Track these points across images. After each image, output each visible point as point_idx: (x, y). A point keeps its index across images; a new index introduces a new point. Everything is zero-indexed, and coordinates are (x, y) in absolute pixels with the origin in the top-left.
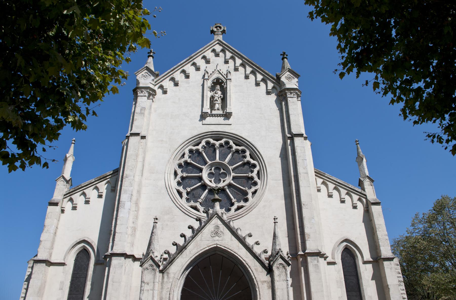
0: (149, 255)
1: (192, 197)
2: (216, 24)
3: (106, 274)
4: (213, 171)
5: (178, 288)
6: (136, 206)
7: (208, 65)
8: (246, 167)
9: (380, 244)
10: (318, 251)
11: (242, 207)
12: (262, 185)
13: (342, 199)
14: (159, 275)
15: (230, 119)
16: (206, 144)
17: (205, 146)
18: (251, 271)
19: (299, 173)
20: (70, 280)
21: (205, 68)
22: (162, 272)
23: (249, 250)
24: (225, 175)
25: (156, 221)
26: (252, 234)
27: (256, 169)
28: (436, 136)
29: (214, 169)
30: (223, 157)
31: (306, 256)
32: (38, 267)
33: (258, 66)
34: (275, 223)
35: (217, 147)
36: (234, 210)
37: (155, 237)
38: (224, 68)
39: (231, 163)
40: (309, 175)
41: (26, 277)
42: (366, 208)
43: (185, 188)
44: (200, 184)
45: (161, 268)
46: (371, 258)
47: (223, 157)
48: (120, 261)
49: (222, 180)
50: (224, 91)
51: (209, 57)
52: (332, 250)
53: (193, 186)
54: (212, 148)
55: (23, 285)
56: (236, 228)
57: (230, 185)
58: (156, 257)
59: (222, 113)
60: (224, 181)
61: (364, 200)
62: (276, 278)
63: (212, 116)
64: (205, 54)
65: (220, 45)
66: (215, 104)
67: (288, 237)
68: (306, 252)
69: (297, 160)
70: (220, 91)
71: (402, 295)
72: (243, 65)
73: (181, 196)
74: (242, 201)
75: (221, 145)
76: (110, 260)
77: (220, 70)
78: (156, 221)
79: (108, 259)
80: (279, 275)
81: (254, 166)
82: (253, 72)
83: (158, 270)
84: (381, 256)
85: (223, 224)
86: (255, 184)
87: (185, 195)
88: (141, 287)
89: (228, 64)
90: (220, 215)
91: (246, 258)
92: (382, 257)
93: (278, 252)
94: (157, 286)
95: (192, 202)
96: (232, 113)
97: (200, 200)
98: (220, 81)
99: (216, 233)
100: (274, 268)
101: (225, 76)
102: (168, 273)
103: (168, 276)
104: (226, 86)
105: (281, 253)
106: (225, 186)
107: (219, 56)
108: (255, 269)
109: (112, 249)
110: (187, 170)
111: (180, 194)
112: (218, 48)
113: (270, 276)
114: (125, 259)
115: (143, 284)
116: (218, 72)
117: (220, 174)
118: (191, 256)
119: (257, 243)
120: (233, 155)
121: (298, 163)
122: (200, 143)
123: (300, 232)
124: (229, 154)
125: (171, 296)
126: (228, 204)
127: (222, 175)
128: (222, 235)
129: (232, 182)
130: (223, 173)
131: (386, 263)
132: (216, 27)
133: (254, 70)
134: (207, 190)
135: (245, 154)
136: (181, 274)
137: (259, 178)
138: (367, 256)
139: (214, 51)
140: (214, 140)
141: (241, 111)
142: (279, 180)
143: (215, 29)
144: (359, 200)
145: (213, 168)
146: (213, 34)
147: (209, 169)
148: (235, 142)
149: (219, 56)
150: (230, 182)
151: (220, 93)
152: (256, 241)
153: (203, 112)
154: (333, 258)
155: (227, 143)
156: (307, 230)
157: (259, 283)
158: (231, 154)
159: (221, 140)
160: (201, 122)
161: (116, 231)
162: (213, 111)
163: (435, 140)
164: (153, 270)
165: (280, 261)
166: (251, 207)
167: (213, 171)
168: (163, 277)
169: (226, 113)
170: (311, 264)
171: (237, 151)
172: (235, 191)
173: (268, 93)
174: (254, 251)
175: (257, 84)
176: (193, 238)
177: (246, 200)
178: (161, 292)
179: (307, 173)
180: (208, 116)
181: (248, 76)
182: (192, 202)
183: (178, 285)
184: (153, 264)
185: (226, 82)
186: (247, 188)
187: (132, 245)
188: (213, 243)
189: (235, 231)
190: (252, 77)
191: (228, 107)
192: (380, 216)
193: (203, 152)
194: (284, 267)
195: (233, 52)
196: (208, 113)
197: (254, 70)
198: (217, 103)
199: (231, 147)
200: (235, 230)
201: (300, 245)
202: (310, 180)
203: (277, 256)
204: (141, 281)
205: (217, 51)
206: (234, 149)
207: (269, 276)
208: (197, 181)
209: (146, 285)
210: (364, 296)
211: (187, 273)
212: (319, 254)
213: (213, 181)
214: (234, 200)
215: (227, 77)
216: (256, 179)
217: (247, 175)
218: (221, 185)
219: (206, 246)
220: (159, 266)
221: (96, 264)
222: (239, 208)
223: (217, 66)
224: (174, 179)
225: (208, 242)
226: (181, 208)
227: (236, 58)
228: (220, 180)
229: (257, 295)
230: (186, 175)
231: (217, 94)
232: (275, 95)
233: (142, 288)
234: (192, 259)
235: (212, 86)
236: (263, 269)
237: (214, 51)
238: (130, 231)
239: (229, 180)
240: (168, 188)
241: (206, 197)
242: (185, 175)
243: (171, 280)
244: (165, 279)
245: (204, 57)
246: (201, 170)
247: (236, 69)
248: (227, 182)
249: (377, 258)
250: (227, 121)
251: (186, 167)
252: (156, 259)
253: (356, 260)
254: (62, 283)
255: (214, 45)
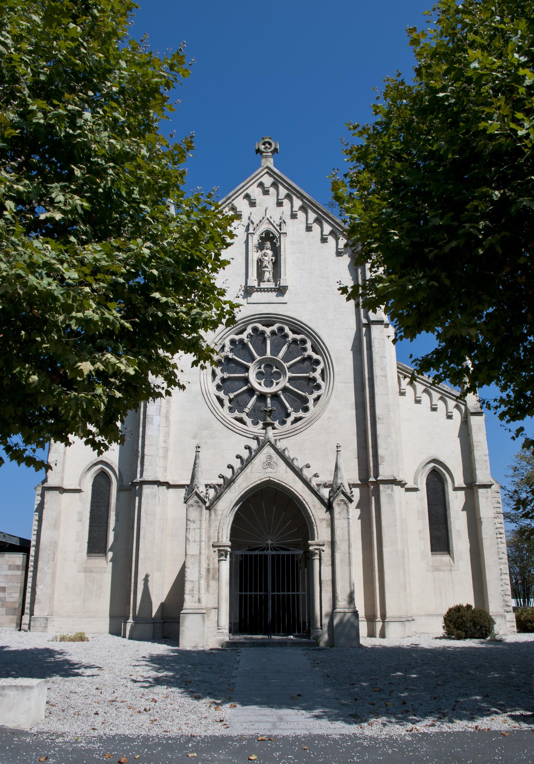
0: (193, 490)
1: (236, 405)
2: (263, 139)
3: (137, 504)
4: (262, 370)
5: (227, 526)
6: (166, 420)
7: (253, 209)
8: (307, 363)
9: (477, 466)
10: (393, 478)
11: (300, 418)
12: (327, 389)
13: (433, 406)
14: (205, 512)
15: (285, 295)
16: (252, 332)
17: (252, 334)
18: (308, 508)
19: (375, 375)
20: (89, 510)
21: (249, 215)
22: (208, 508)
23: (306, 483)
24: (278, 375)
25: (199, 450)
26: (311, 464)
27: (319, 366)
28: (486, 402)
29: (264, 367)
30: (276, 350)
31: (377, 483)
32: (49, 495)
33: (325, 211)
34: (337, 451)
35: (268, 335)
36: (290, 423)
37: (199, 469)
38: (275, 214)
39: (286, 358)
40: (389, 379)
41: (36, 507)
42: (464, 418)
43: (226, 393)
44: (245, 388)
45: (207, 505)
46: (465, 483)
47: (276, 350)
48: (153, 490)
49: (275, 381)
50: (276, 251)
51: (254, 196)
52: (415, 473)
53: (237, 390)
54: (260, 337)
55: (33, 516)
56: (292, 458)
57: (285, 390)
58: (202, 492)
59: (274, 286)
60: (277, 384)
61: (463, 407)
62: (336, 516)
63: (261, 291)
64: (248, 191)
65: (270, 175)
66: (264, 272)
67: (358, 458)
68: (379, 478)
69: (374, 358)
70: (271, 250)
71: (498, 530)
72: (303, 208)
73: (222, 405)
74: (301, 411)
75: (273, 333)
76: (141, 489)
77: (271, 217)
78: (199, 450)
79: (137, 487)
80: (340, 513)
81: (317, 362)
82: (318, 221)
83: (204, 507)
84: (476, 482)
85: (277, 453)
86: (318, 387)
87: (227, 404)
88: (187, 525)
89: (282, 206)
90: (273, 442)
91: (303, 493)
92: (477, 484)
93: (340, 487)
94: (204, 524)
95: (236, 412)
96: (287, 286)
97: (247, 410)
98: (271, 235)
99: (269, 464)
100: (335, 505)
101: (278, 228)
102: (215, 510)
103: (215, 513)
104: (279, 243)
105: (342, 488)
106: (278, 391)
107: (269, 194)
108: (313, 506)
109: (141, 475)
110: (228, 369)
111: (221, 401)
112: (267, 181)
113: (330, 514)
114: (158, 487)
115: (189, 522)
116: (267, 221)
117: (272, 374)
118: (241, 490)
119: (316, 476)
120: (289, 347)
121: (374, 362)
122: (245, 330)
123: (373, 453)
124: (284, 345)
125: (220, 535)
126: (283, 414)
127: (274, 375)
128: (275, 466)
129: (288, 385)
130: (275, 372)
131: (481, 491)
132: (264, 144)
133: (320, 217)
134: (255, 397)
135: (306, 345)
136: (230, 511)
137: (323, 380)
138: (460, 481)
139: (261, 185)
140: (263, 325)
141: (300, 282)
142: (350, 383)
143: (262, 147)
144: (457, 407)
145: (263, 366)
146: (259, 154)
147: (257, 367)
148: (292, 328)
149: (269, 194)
150: (285, 386)
151: (270, 253)
152: (315, 473)
153: (248, 285)
154: (415, 483)
155: (281, 329)
156: (380, 452)
157: (317, 521)
158: (286, 346)
159: (273, 325)
160: (246, 299)
161: (145, 453)
162: (262, 283)
163: (485, 405)
164: (199, 506)
165: (342, 497)
166: (312, 419)
167: (262, 370)
168: (210, 515)
169: (280, 287)
170: (384, 493)
171: (295, 341)
172: (292, 396)
173: (339, 254)
174: (312, 485)
175: (324, 240)
176: (242, 469)
177: (306, 410)
178: (209, 531)
179: (385, 376)
180: (255, 291)
181: (311, 227)
182: (236, 412)
183: (227, 523)
184: (199, 500)
185: (280, 237)
186: (307, 394)
187: (165, 469)
188: (266, 476)
189: (291, 462)
190: (316, 227)
191: (282, 277)
192: (480, 430)
193: (249, 343)
194: (345, 503)
195: (290, 188)
196: (254, 287)
197: (320, 217)
198: (267, 271)
199: (286, 336)
200: (290, 461)
201: (372, 470)
202: (389, 385)
203: (338, 491)
204: (187, 520)
205: (265, 186)
206: (290, 339)
207: (328, 513)
208: (241, 383)
209: (192, 523)
210: (451, 530)
211: (236, 509)
212: (394, 482)
213: (262, 384)
214: (290, 410)
215: (280, 229)
216: (319, 381)
217: (308, 375)
218: (274, 389)
219: (257, 479)
220: (205, 503)
221: (120, 489)
222: (297, 420)
223: (266, 210)
224: (213, 382)
225: (259, 475)
226: (223, 421)
227: (294, 198)
228: (272, 383)
229: (314, 534)
230: (228, 375)
231: (266, 256)
232: (349, 256)
233: (188, 527)
234: (241, 494)
235: (259, 243)
236: (322, 506)
237: (261, 185)
238: (161, 452)
239: (284, 382)
240: (204, 394)
241: (254, 406)
242: (226, 375)
243: (219, 518)
244: (213, 517)
245: (247, 196)
246: (247, 369)
247: (294, 216)
248: (281, 386)
249: (472, 484)
250: (281, 297)
251: (227, 365)
252: (202, 495)
253: (445, 486)
254: (80, 513)
255: (262, 176)
